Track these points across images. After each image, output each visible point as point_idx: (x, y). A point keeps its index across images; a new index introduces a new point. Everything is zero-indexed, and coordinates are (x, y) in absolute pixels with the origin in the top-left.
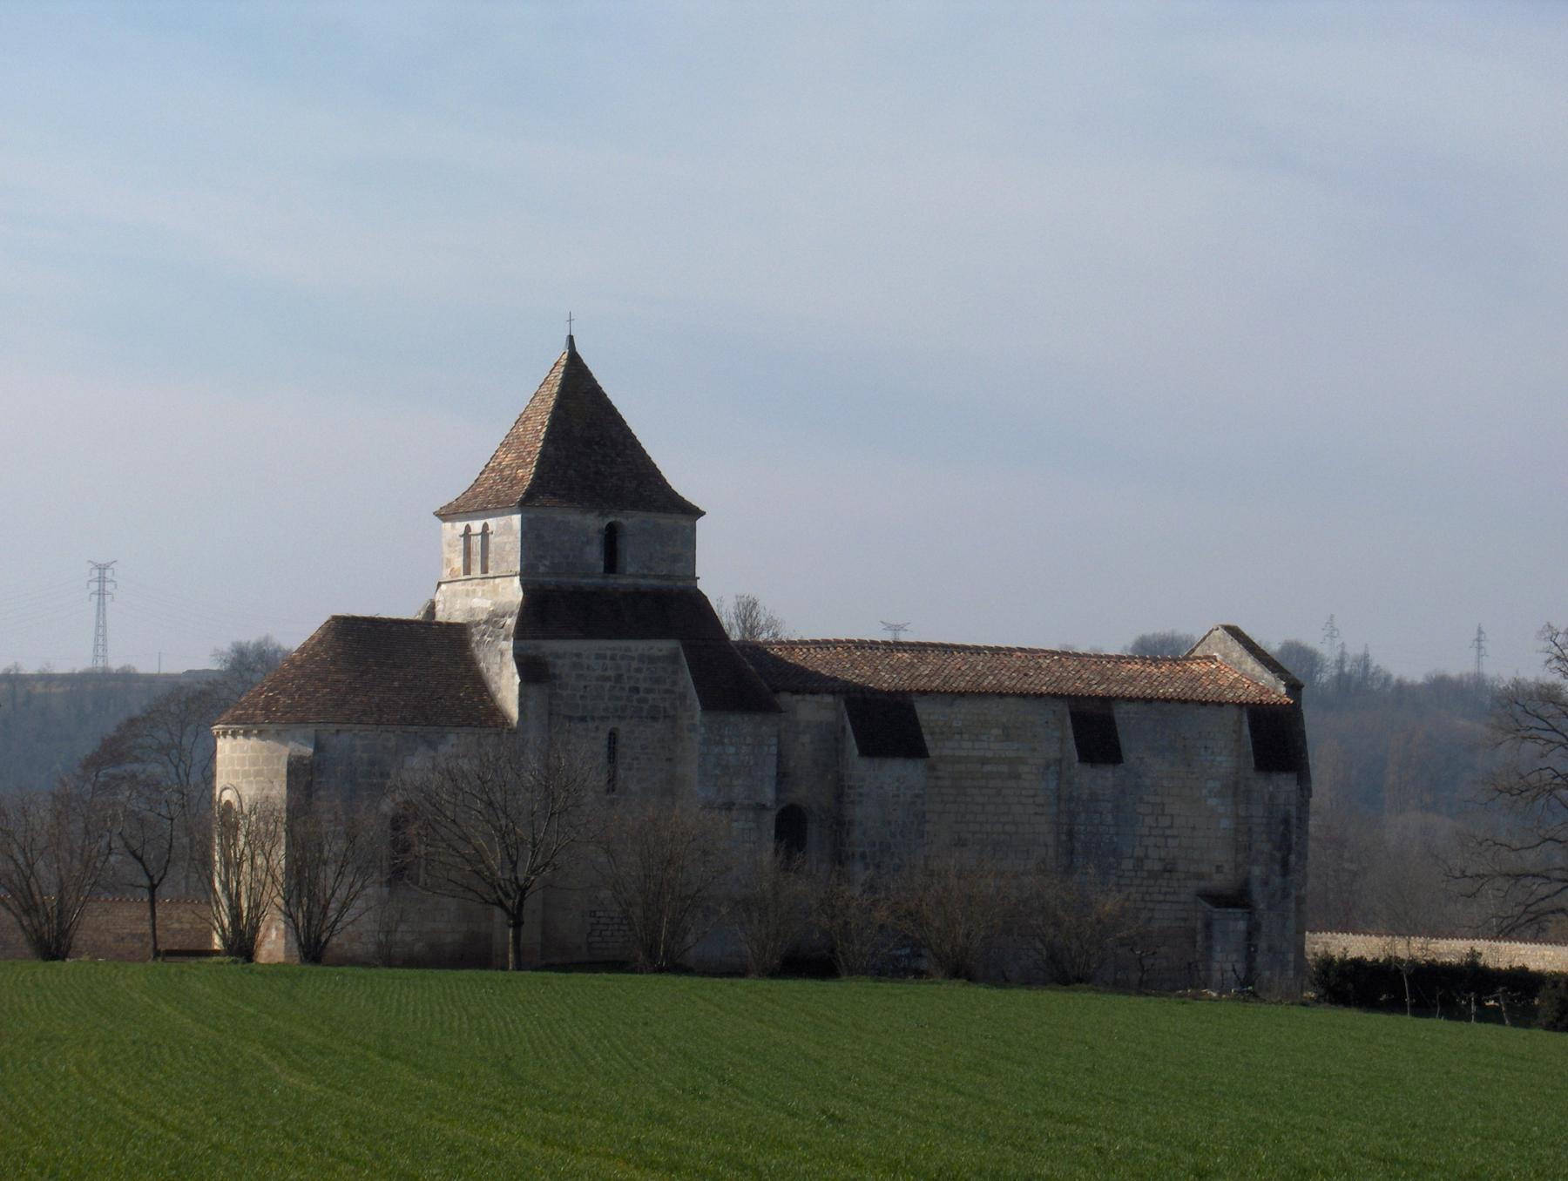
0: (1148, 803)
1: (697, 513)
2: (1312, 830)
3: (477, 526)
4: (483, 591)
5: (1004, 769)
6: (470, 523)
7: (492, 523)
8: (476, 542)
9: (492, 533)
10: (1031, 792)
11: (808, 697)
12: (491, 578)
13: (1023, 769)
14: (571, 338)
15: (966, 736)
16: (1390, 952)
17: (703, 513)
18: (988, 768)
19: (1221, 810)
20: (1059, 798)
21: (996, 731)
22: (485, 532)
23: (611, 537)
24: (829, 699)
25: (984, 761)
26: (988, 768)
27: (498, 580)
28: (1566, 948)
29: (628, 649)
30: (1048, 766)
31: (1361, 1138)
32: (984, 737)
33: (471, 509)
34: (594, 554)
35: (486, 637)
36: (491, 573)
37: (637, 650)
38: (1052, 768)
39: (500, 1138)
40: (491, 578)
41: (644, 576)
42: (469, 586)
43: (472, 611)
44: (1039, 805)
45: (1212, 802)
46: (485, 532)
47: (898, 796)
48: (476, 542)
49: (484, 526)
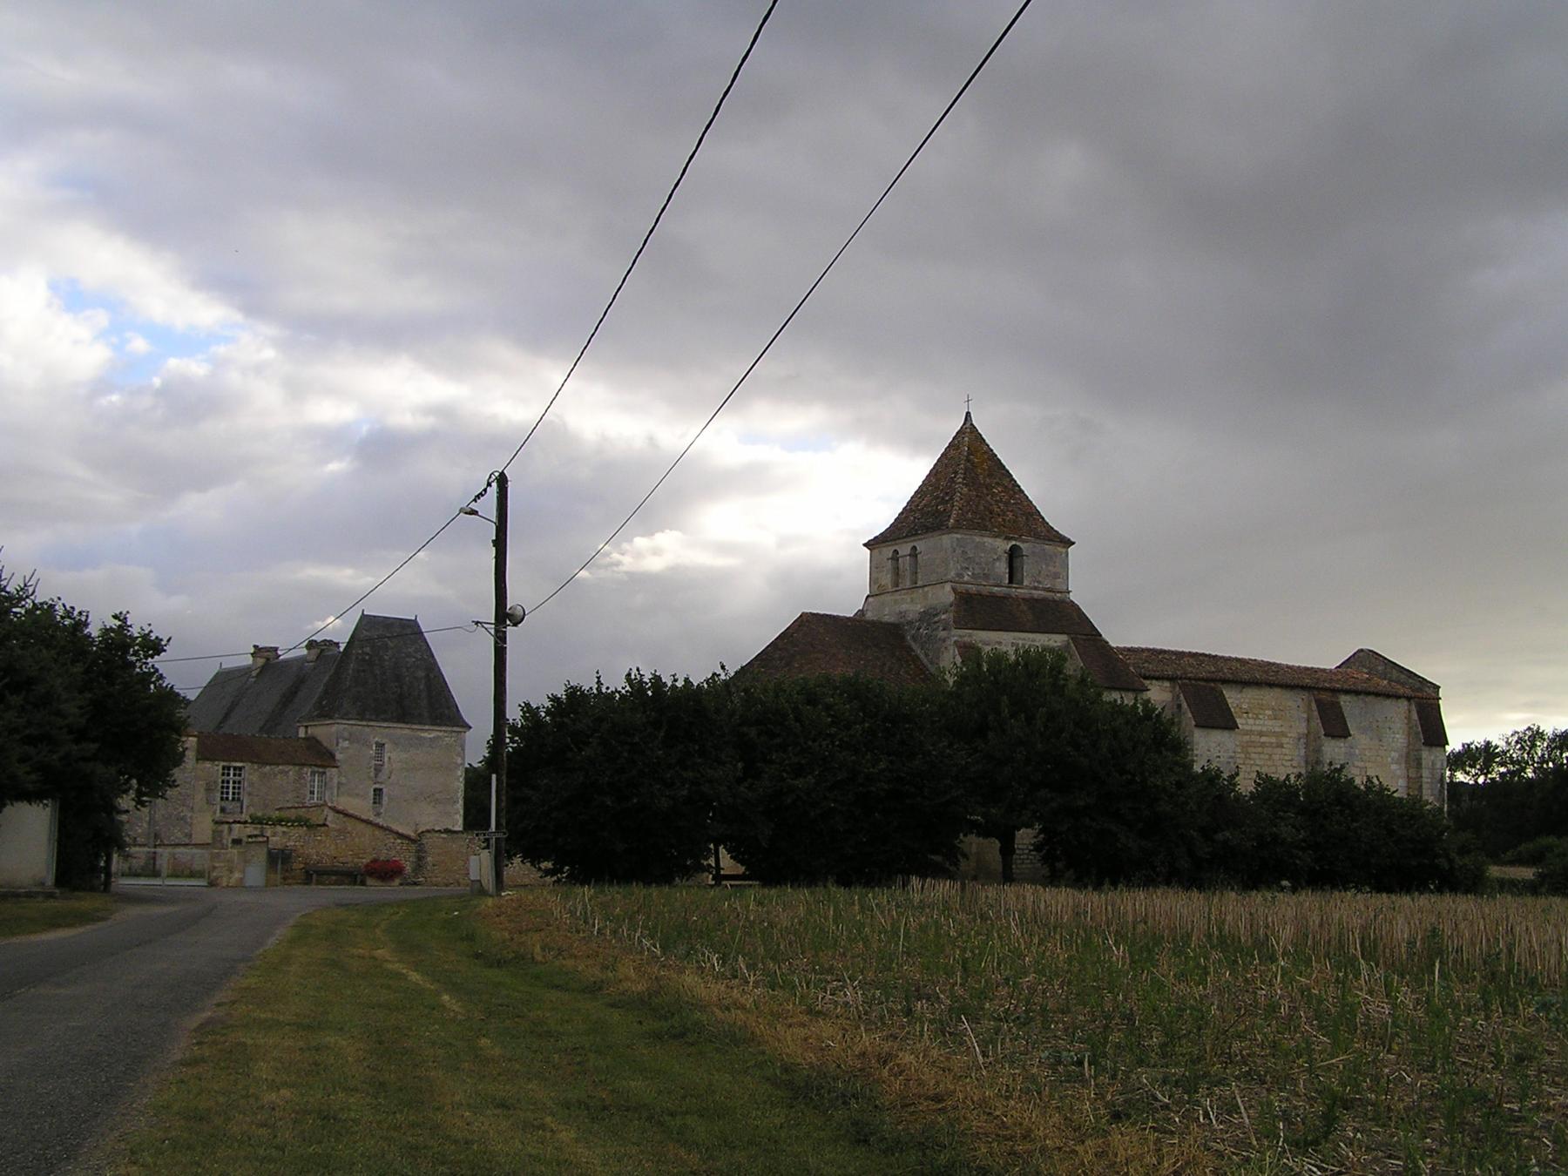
0: (1357, 767)
1: (1069, 543)
2: (505, 879)
3: (905, 549)
4: (912, 598)
5: (1273, 740)
6: (915, 544)
7: (920, 546)
8: (905, 563)
9: (921, 553)
10: (1290, 758)
11: (1154, 682)
12: (920, 587)
13: (1284, 740)
14: (968, 414)
15: (1250, 715)
16: (1479, 901)
17: (865, 545)
18: (1263, 739)
19: (1398, 772)
20: (1307, 762)
21: (1269, 712)
22: (914, 553)
23: (1013, 554)
24: (1167, 684)
25: (1261, 734)
26: (1263, 739)
27: (926, 589)
28: (1566, 901)
29: (1034, 640)
30: (1299, 739)
31: (1366, 1075)
32: (1261, 717)
33: (901, 536)
34: (1002, 568)
35: (921, 630)
36: (920, 583)
37: (1040, 640)
38: (1302, 740)
39: (105, 1162)
40: (920, 587)
41: (1036, 588)
42: (897, 596)
43: (902, 614)
44: (1294, 767)
45: (1394, 767)
46: (914, 553)
47: (1219, 757)
48: (905, 563)
49: (912, 548)
